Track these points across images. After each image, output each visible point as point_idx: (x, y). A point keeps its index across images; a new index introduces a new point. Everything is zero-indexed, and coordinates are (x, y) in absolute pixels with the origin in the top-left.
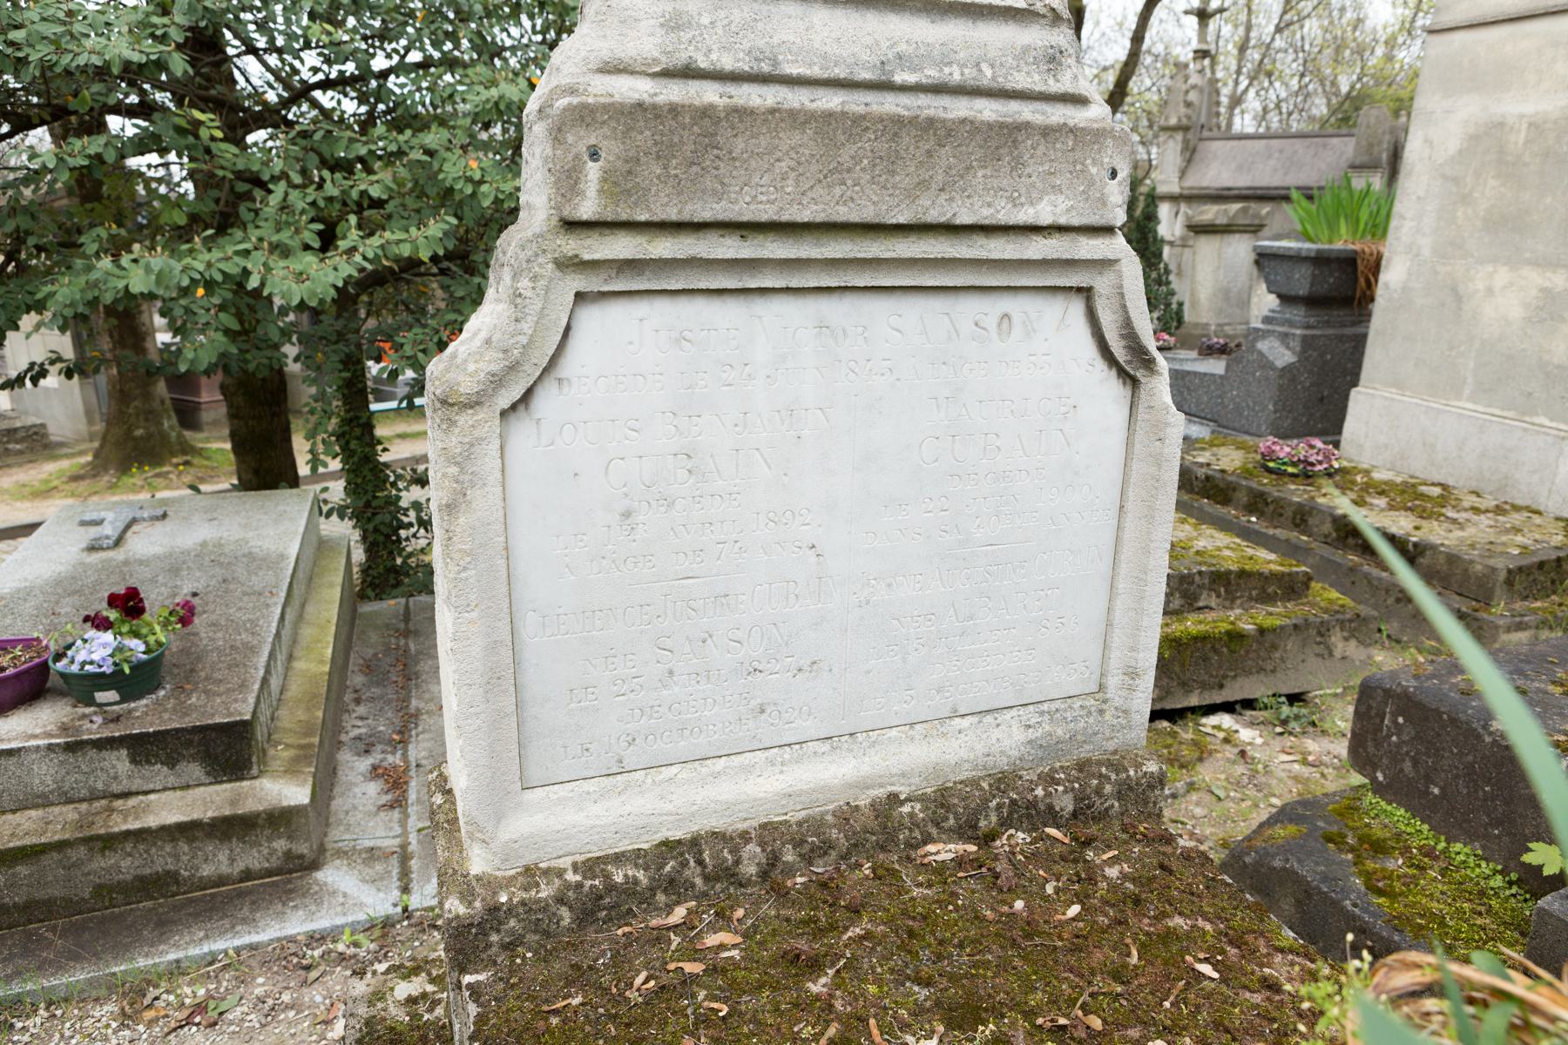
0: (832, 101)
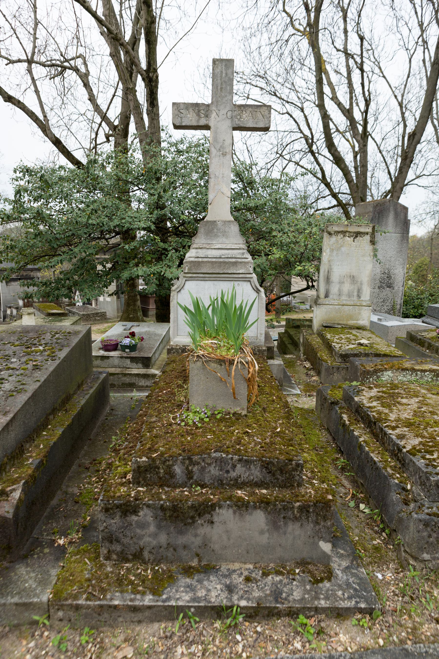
0: (214, 260)
